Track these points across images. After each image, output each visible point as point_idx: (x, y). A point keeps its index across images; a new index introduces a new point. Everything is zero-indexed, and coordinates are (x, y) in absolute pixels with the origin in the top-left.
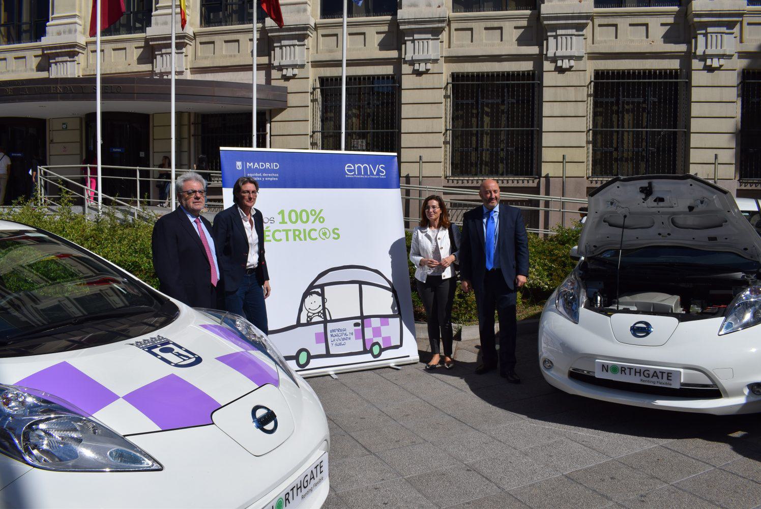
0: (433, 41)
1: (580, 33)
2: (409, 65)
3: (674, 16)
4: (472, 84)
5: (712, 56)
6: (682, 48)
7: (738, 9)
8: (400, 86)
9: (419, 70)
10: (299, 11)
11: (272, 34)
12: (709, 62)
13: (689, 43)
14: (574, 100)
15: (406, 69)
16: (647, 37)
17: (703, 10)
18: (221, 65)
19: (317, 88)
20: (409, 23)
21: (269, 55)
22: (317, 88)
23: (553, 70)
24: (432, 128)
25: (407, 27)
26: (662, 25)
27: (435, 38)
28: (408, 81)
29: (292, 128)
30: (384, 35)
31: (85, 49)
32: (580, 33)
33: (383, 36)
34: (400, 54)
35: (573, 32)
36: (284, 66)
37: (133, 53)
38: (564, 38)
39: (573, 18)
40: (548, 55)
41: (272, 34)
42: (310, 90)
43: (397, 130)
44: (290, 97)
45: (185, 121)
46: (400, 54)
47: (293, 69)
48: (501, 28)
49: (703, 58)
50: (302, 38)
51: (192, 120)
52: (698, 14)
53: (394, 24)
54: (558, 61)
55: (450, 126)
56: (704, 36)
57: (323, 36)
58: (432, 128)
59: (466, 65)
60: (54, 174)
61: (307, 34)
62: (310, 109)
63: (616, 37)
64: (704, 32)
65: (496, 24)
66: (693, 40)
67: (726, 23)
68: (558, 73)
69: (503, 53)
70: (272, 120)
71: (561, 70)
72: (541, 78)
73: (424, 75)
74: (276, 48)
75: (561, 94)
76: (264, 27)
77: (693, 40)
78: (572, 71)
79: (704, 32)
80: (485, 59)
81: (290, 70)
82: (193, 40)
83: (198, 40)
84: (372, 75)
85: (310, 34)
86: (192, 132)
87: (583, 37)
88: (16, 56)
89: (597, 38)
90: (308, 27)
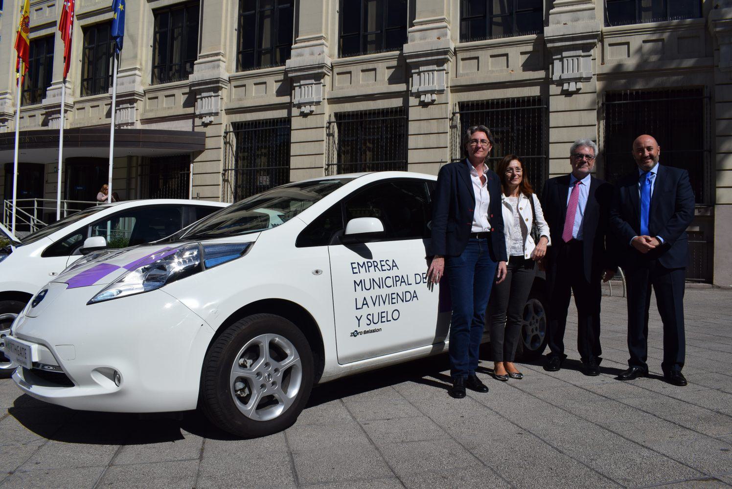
0: (316, 85)
1: (441, 68)
2: (415, 98)
3: (397, 59)
4: (507, 111)
5: (569, 81)
6: (541, 74)
7: (591, 31)
8: (548, 108)
9: (568, 90)
10: (214, 67)
11: (194, 88)
12: (566, 86)
13: (546, 69)
14: (436, 132)
15: (413, 101)
16: (508, 67)
17: (554, 35)
18: (161, 116)
19: (457, 113)
20: (296, 71)
21: (407, 83)
22: (457, 113)
23: (418, 105)
24: (315, 163)
25: (294, 74)
26: (522, 53)
27: (318, 82)
28: (414, 113)
29: (208, 167)
30: (281, 83)
31: (73, 107)
32: (441, 68)
33: (280, 83)
34: (408, 87)
35: (435, 67)
36: (203, 114)
37: (104, 109)
38: (426, 73)
39: (432, 54)
40: (554, 79)
41: (194, 88)
42: (450, 116)
43: (404, 161)
44: (207, 140)
45: (134, 164)
46: (408, 87)
47: (310, 106)
48: (507, 55)
49: (560, 82)
50: (217, 90)
51: (140, 162)
52: (550, 39)
53: (402, 58)
54: (422, 96)
55: (232, 164)
56: (560, 61)
57: (463, 59)
58: (315, 163)
59: (346, 105)
60: (21, 210)
61: (219, 86)
62: (325, 144)
63: (478, 70)
64: (559, 56)
65: (371, 66)
66: (551, 66)
67: (566, 47)
68: (204, 127)
69: (376, 92)
70: (194, 161)
71: (424, 105)
72: (547, 103)
73: (309, 117)
74: (555, 61)
75: (425, 127)
76: (401, 55)
77: (551, 66)
78: (435, 104)
79: (559, 56)
80: (361, 98)
81: (308, 107)
82: (143, 96)
83: (460, 55)
84: (244, 121)
85: (450, 59)
86: (139, 172)
87: (445, 72)
88: (255, 82)
89: (461, 71)
90: (324, 66)
